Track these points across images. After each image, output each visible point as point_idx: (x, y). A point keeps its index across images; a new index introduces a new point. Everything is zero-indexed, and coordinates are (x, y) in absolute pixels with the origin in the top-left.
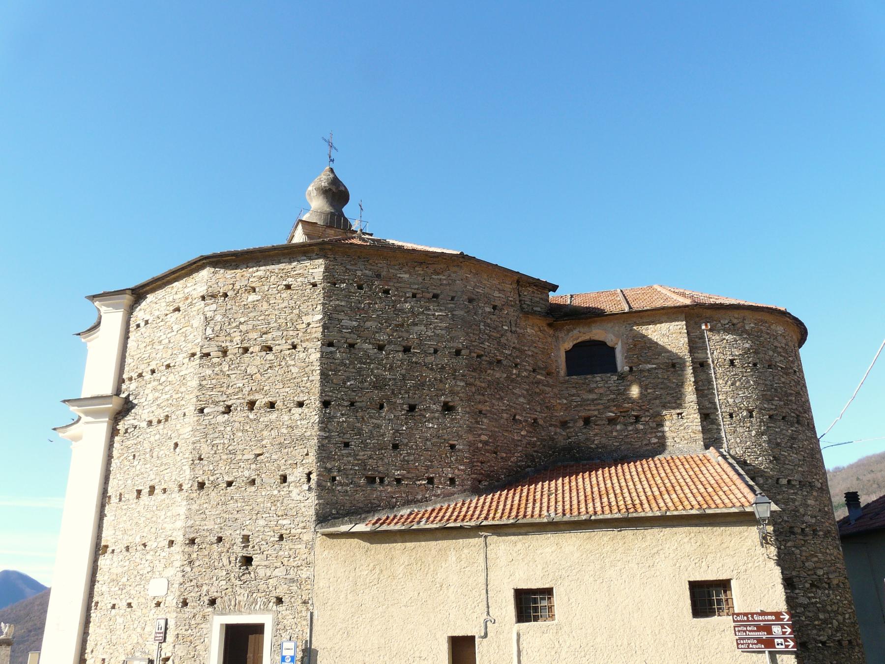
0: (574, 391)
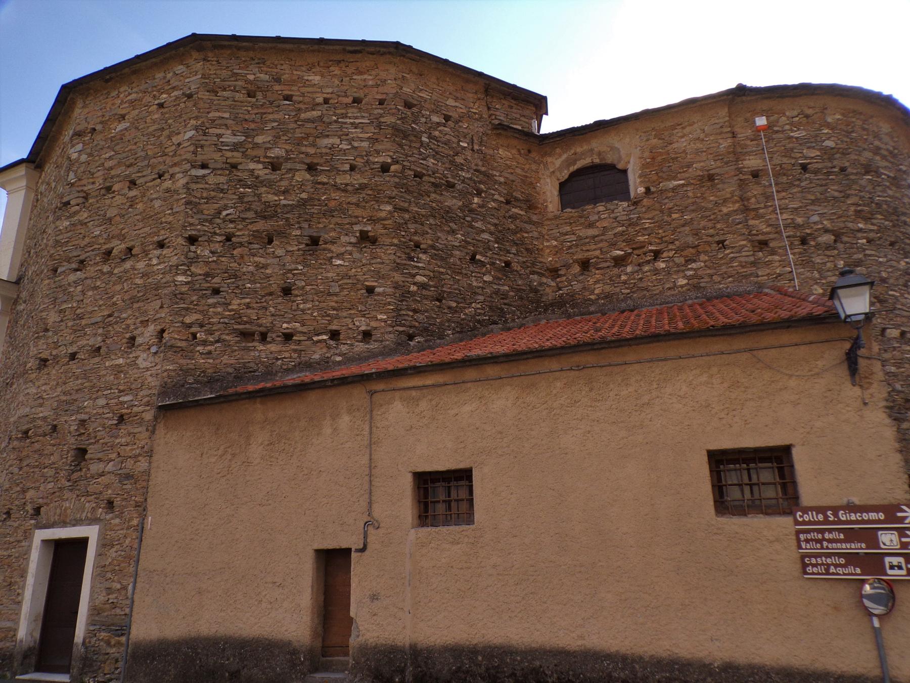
0: (568, 228)
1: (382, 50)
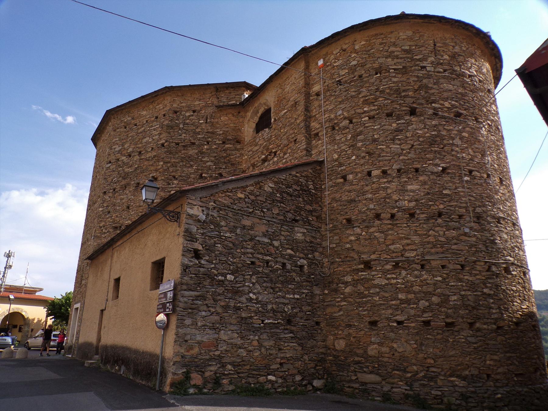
1: (164, 91)
